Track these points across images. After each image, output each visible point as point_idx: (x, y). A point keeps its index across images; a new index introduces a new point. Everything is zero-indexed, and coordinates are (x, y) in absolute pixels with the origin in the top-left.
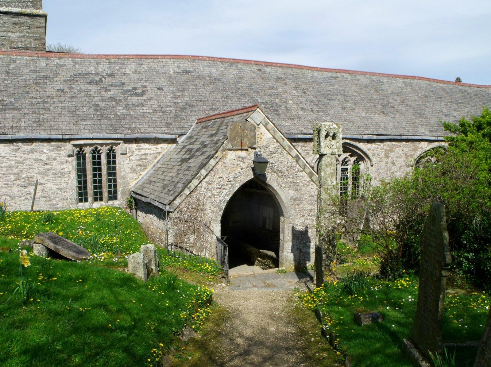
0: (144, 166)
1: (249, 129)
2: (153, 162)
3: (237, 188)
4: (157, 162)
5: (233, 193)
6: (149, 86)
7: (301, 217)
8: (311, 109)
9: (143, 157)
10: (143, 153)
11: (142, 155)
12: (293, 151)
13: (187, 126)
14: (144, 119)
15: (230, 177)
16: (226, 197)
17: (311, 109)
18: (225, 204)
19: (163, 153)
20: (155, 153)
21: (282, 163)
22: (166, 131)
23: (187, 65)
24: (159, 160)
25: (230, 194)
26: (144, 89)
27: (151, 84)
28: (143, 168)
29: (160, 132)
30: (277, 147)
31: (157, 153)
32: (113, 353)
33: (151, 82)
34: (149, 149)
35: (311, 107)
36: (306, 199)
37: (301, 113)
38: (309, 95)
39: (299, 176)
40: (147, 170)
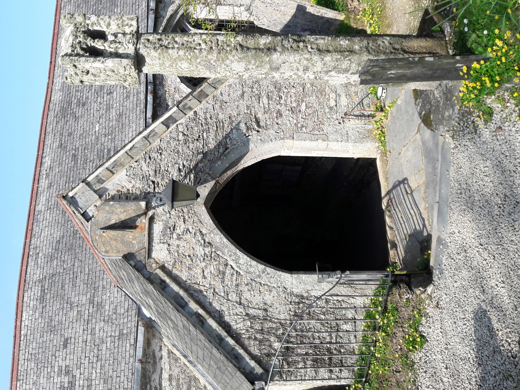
0: (190, 382)
1: (109, 216)
2: (185, 364)
3: (225, 240)
4: (185, 357)
5: (232, 248)
6: (60, 362)
7: (281, 115)
8: (108, 95)
9: (174, 384)
10: (168, 383)
11: (171, 384)
12: (156, 130)
13: (127, 304)
14: (110, 379)
15: (203, 253)
16: (241, 261)
17: (108, 95)
18: (254, 263)
19: (170, 347)
20: (170, 361)
21: (178, 152)
22: (132, 341)
23: (32, 294)
24: (181, 353)
25: (235, 254)
26: (63, 372)
27: (58, 359)
28: (193, 383)
29: (132, 352)
30: (148, 160)
31: (169, 357)
32: (268, 41)
33: (54, 357)
34: (161, 373)
35: (105, 95)
36: (248, 107)
37: (113, 113)
38: (87, 98)
39: (206, 119)
40: (198, 376)
